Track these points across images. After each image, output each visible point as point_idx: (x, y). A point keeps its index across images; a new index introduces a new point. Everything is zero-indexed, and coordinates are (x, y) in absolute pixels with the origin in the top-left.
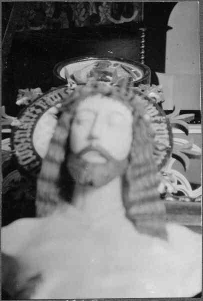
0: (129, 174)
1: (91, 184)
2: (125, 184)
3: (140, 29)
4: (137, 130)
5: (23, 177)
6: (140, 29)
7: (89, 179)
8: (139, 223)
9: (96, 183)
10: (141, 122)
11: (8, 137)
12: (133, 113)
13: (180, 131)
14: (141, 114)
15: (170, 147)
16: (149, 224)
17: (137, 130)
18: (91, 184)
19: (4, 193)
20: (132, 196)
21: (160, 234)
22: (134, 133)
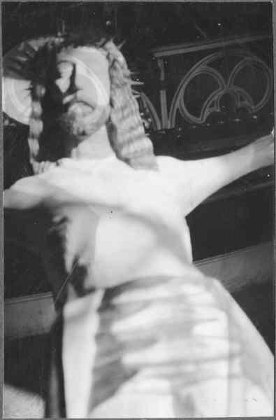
0: (115, 120)
1: (84, 134)
2: (111, 129)
3: (142, 83)
4: (114, 73)
5: (132, 73)
6: (142, 83)
7: (81, 130)
8: (132, 161)
9: (88, 132)
10: (117, 65)
11: (27, 79)
12: (108, 57)
13: (110, 56)
14: (116, 58)
15: (184, 392)
16: (140, 160)
17: (114, 73)
18: (84, 134)
19: (64, 115)
20: (120, 138)
21: (152, 166)
22: (111, 78)
